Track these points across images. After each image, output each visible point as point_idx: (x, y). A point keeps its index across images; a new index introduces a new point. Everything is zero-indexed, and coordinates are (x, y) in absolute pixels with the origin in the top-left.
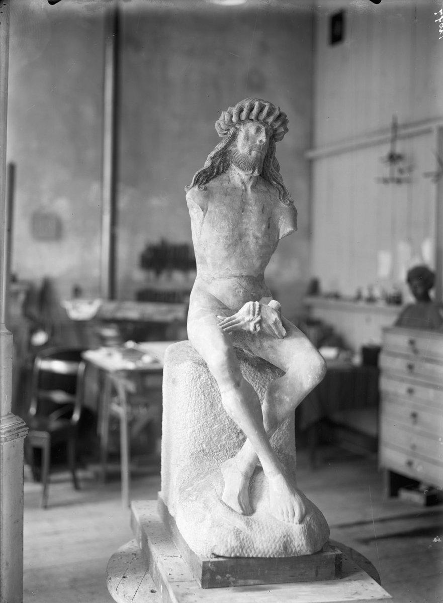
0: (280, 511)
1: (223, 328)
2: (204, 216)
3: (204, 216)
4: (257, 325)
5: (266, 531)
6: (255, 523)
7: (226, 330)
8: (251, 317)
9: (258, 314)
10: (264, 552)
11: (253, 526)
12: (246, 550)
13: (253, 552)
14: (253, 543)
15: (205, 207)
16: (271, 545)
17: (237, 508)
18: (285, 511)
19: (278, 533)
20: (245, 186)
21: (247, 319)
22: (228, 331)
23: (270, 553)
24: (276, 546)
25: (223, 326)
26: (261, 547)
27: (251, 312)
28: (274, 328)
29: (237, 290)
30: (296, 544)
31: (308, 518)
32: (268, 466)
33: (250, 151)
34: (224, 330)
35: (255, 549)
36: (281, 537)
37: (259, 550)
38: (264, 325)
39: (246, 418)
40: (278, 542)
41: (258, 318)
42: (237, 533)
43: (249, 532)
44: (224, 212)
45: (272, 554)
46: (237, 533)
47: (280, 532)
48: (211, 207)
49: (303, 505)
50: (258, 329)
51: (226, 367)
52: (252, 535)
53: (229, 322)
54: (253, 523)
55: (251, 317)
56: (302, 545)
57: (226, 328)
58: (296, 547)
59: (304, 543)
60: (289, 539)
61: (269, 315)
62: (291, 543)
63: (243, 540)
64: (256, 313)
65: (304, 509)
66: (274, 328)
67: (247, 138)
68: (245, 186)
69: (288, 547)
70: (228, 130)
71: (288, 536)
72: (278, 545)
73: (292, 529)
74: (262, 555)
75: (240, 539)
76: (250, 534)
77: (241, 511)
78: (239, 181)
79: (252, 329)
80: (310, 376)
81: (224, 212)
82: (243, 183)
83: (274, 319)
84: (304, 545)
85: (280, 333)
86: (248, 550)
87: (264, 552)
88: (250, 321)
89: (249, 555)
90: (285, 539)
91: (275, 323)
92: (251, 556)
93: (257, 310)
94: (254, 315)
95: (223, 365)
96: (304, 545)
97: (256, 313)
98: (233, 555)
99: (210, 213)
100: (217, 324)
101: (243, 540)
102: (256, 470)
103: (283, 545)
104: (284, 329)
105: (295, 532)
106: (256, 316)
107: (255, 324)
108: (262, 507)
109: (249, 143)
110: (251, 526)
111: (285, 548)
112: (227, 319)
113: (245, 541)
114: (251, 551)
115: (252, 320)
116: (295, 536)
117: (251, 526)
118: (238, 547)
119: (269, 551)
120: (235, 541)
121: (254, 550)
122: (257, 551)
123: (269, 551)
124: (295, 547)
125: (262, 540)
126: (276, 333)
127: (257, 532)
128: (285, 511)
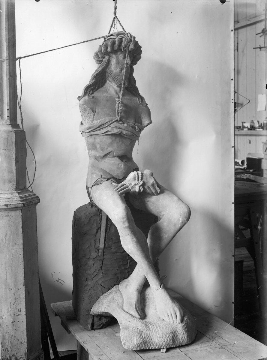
0: (166, 315)
1: (119, 192)
2: (94, 115)
3: (94, 115)
4: (141, 187)
5: (160, 330)
6: (151, 325)
7: (121, 193)
8: (136, 182)
9: (141, 180)
10: (160, 345)
11: (150, 327)
12: (148, 345)
13: (152, 346)
14: (151, 339)
15: (94, 109)
16: (164, 340)
17: (135, 313)
18: (169, 315)
19: (169, 330)
20: (118, 95)
21: (133, 183)
22: (122, 194)
23: (164, 345)
24: (168, 340)
25: (118, 190)
26: (157, 342)
27: (136, 179)
28: (151, 188)
29: (119, 165)
30: (180, 337)
31: (185, 319)
32: (154, 283)
33: (121, 70)
34: (119, 193)
35: (153, 343)
36: (170, 333)
37: (156, 343)
38: (146, 187)
39: (140, 253)
40: (168, 337)
41: (142, 183)
42: (140, 333)
43: (148, 332)
44: (107, 112)
45: (165, 345)
46: (140, 333)
47: (169, 330)
48: (98, 110)
49: (181, 309)
50: (142, 190)
51: (125, 219)
52: (150, 333)
53: (122, 187)
54: (150, 324)
55: (136, 182)
56: (184, 338)
57: (121, 192)
58: (180, 339)
59: (186, 336)
60: (175, 334)
61: (148, 179)
62: (177, 337)
63: (145, 337)
64: (140, 179)
65: (182, 312)
66: (151, 188)
67: (118, 62)
68: (118, 95)
69: (175, 340)
70: (104, 58)
71: (175, 332)
72: (168, 339)
73: (177, 328)
74: (158, 347)
75: (143, 337)
76: (149, 333)
77: (139, 317)
78: (114, 91)
79: (137, 190)
80: (181, 219)
81: (107, 112)
82: (116, 92)
83: (152, 182)
84: (186, 338)
85: (156, 191)
86: (149, 344)
87: (160, 345)
88: (135, 185)
89: (149, 347)
90: (173, 335)
91: (153, 185)
92: (151, 348)
93: (140, 177)
94: (138, 180)
95: (123, 218)
96: (186, 338)
97: (140, 179)
98: (138, 349)
99: (98, 113)
100: (113, 189)
101: (145, 337)
102: (146, 285)
103: (172, 339)
104: (158, 188)
105: (179, 329)
106: (140, 181)
107: (139, 187)
108: (150, 311)
109: (120, 65)
110: (148, 327)
111: (174, 341)
112: (120, 185)
113: (146, 338)
114: (151, 345)
115: (137, 184)
116: (179, 332)
117: (148, 327)
118: (142, 343)
119: (163, 344)
120: (140, 338)
121: (153, 344)
122: (155, 344)
123: (163, 344)
124: (179, 339)
125: (157, 337)
126: (154, 192)
127: (153, 331)
128: (169, 315)
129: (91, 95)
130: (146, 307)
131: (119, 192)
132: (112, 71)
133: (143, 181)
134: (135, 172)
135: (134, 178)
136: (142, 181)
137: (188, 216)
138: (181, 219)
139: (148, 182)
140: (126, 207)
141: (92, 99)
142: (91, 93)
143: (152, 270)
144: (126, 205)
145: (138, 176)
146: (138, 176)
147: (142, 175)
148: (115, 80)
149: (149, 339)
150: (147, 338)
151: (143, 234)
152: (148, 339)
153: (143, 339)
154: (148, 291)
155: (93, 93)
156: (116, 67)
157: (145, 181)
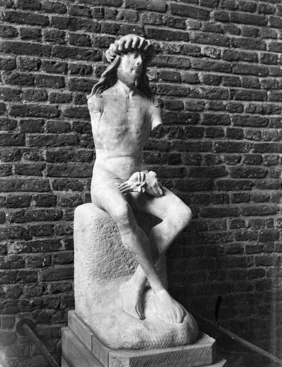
1: (120, 190)
9: (144, 180)
27: (139, 179)
29: (125, 166)
31: (185, 319)
34: (121, 191)
41: (144, 183)
50: (144, 191)
53: (124, 187)
55: (138, 182)
67: (129, 62)
68: (128, 94)
71: (174, 332)
82: (126, 92)
93: (142, 177)
94: (140, 181)
95: (124, 215)
97: (142, 179)
101: (144, 336)
104: (161, 190)
106: (142, 182)
119: (161, 344)
123: (161, 344)
127: (153, 331)
129: (100, 93)
130: (146, 303)
131: (120, 190)
132: (122, 70)
133: (145, 182)
134: (138, 173)
135: (137, 179)
136: (144, 182)
137: (189, 219)
138: (181, 221)
139: (150, 183)
140: (127, 205)
141: (100, 99)
142: (100, 91)
143: (153, 270)
144: (127, 203)
145: (140, 177)
146: (140, 177)
147: (144, 176)
148: (124, 82)
149: (148, 338)
150: (146, 337)
151: (137, 226)
152: (147, 338)
153: (142, 339)
154: (150, 293)
155: (102, 92)
156: (127, 66)
157: (147, 182)
